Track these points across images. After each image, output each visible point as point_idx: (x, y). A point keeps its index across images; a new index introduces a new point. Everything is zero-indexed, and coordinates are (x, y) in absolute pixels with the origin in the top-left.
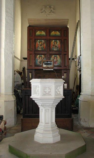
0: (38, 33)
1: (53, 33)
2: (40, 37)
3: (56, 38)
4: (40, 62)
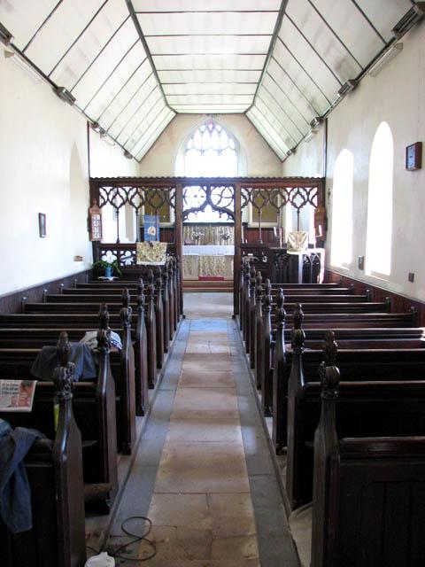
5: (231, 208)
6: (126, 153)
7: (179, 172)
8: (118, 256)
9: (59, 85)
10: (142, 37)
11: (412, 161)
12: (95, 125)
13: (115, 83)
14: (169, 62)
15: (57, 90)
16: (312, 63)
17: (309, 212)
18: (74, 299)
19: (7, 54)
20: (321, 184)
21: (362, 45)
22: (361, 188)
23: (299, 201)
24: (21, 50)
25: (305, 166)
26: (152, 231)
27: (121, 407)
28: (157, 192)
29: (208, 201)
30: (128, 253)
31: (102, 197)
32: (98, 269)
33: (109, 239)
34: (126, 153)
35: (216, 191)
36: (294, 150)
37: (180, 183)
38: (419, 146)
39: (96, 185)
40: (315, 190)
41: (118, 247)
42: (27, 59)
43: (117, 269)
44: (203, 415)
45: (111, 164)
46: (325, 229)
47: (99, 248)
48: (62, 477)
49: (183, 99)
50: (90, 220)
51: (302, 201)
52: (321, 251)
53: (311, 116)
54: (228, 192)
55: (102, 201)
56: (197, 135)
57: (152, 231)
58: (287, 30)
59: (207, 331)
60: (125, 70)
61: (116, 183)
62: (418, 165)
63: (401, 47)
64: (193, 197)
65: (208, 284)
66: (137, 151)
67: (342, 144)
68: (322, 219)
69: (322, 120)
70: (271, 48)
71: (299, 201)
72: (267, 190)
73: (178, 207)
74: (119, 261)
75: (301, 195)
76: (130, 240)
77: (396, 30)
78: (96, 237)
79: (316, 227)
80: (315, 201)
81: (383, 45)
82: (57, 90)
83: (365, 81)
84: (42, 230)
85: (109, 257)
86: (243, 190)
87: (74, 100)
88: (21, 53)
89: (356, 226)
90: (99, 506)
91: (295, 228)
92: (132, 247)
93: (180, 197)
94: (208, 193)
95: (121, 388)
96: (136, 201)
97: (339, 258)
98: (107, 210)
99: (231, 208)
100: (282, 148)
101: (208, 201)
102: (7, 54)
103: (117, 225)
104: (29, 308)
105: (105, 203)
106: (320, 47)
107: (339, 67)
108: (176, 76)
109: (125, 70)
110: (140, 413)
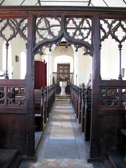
0: (60, 67)
1: (65, 67)
2: (61, 69)
3: (66, 69)
4: (61, 77)
31: (104, 31)
40: (26, 21)
51: (12, 32)
55: (102, 34)
75: (10, 25)
86: (102, 22)
94: (64, 25)
105: (106, 37)
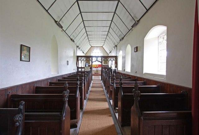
5: (101, 61)
6: (83, 52)
7: (92, 55)
8: (82, 69)
9: (56, 20)
10: (86, 31)
11: (136, 50)
12: (78, 47)
13: (81, 39)
14: (90, 24)
15: (71, 39)
16: (115, 36)
17: (114, 62)
18: (73, 77)
19: (62, 31)
20: (116, 57)
21: (124, 30)
22: (124, 58)
23: (112, 60)
24: (47, 9)
25: (113, 54)
26: (87, 66)
27: (81, 99)
28: (88, 58)
29: (97, 60)
30: (83, 69)
32: (78, 72)
33: (80, 66)
34: (83, 52)
35: (98, 58)
36: (111, 52)
37: (92, 57)
38: (137, 47)
39: (78, 57)
41: (81, 68)
42: (48, 12)
43: (82, 72)
44: (96, 116)
45: (80, 53)
46: (117, 64)
47: (78, 68)
48: (63, 125)
49: (93, 44)
50: (77, 63)
52: (116, 68)
53: (114, 46)
54: (100, 58)
56: (95, 50)
57: (87, 66)
58: (111, 31)
59: (97, 80)
60: (83, 37)
61: (81, 57)
62: (137, 51)
63: (132, 30)
64: (94, 59)
65: (96, 74)
66: (85, 52)
67: (120, 50)
68: (116, 63)
69: (116, 46)
70: (108, 34)
71: (112, 60)
72: (106, 58)
73: (92, 61)
74: (81, 70)
76: (58, 68)
77: (132, 27)
78: (78, 66)
79: (115, 64)
80: (115, 60)
81: (146, 11)
82: (71, 39)
83: (124, 38)
84: (68, 64)
85: (80, 70)
87: (62, 27)
88: (65, 31)
89: (123, 64)
90: (74, 126)
91: (111, 64)
92: (84, 68)
93: (92, 59)
95: (81, 95)
96: (85, 60)
97: (120, 68)
98: (80, 61)
99: (101, 61)
100: (108, 52)
101: (97, 60)
102: (62, 31)
103: (81, 64)
104: (65, 78)
106: (117, 32)
107: (120, 36)
108: (91, 39)
109: (83, 37)
110: (85, 99)
